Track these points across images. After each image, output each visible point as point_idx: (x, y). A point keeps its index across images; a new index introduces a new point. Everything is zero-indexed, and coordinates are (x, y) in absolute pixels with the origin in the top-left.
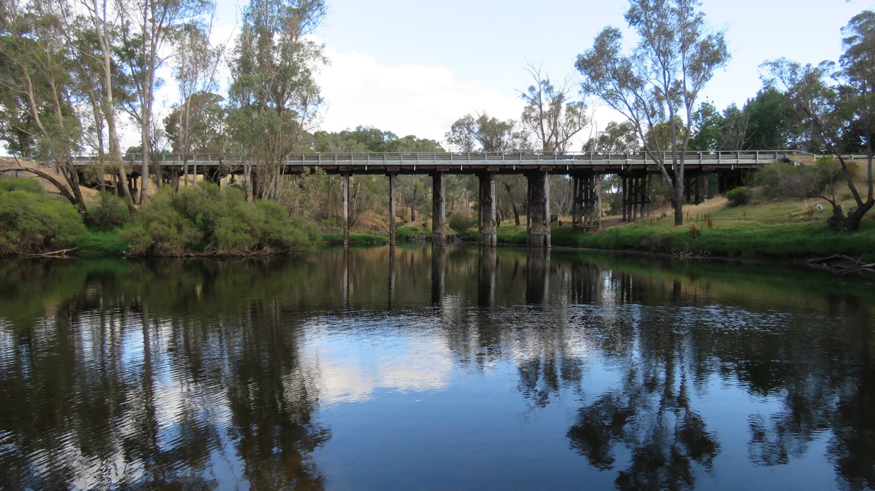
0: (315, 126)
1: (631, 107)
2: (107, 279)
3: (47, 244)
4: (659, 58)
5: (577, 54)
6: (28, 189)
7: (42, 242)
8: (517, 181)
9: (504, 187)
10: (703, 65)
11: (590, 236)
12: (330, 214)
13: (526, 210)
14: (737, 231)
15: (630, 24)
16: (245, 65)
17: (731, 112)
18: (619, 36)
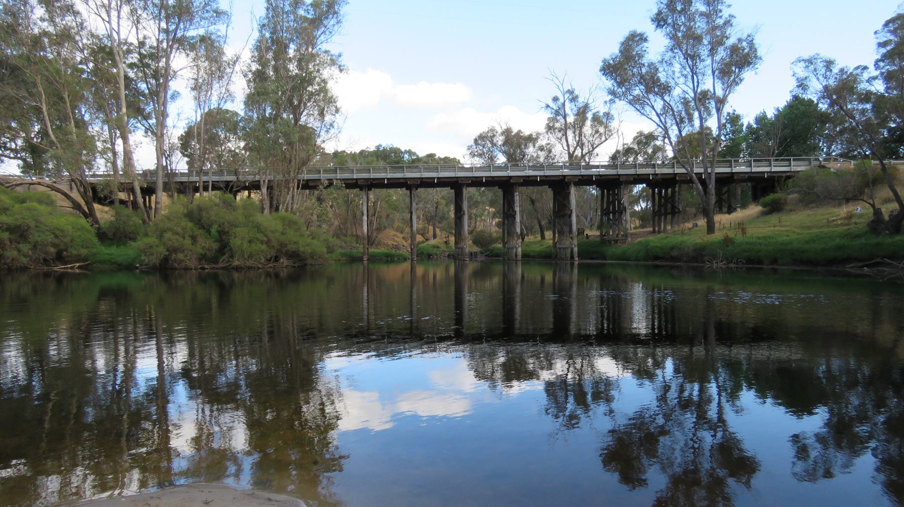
0: (333, 137)
1: (659, 112)
2: (120, 296)
3: (60, 257)
4: (687, 61)
5: (603, 59)
6: (40, 202)
7: (54, 255)
8: (542, 196)
9: (529, 202)
10: (733, 68)
11: (619, 249)
12: (349, 233)
13: (552, 226)
14: (773, 238)
15: (657, 27)
16: (259, 77)
17: (761, 119)
18: (646, 40)
